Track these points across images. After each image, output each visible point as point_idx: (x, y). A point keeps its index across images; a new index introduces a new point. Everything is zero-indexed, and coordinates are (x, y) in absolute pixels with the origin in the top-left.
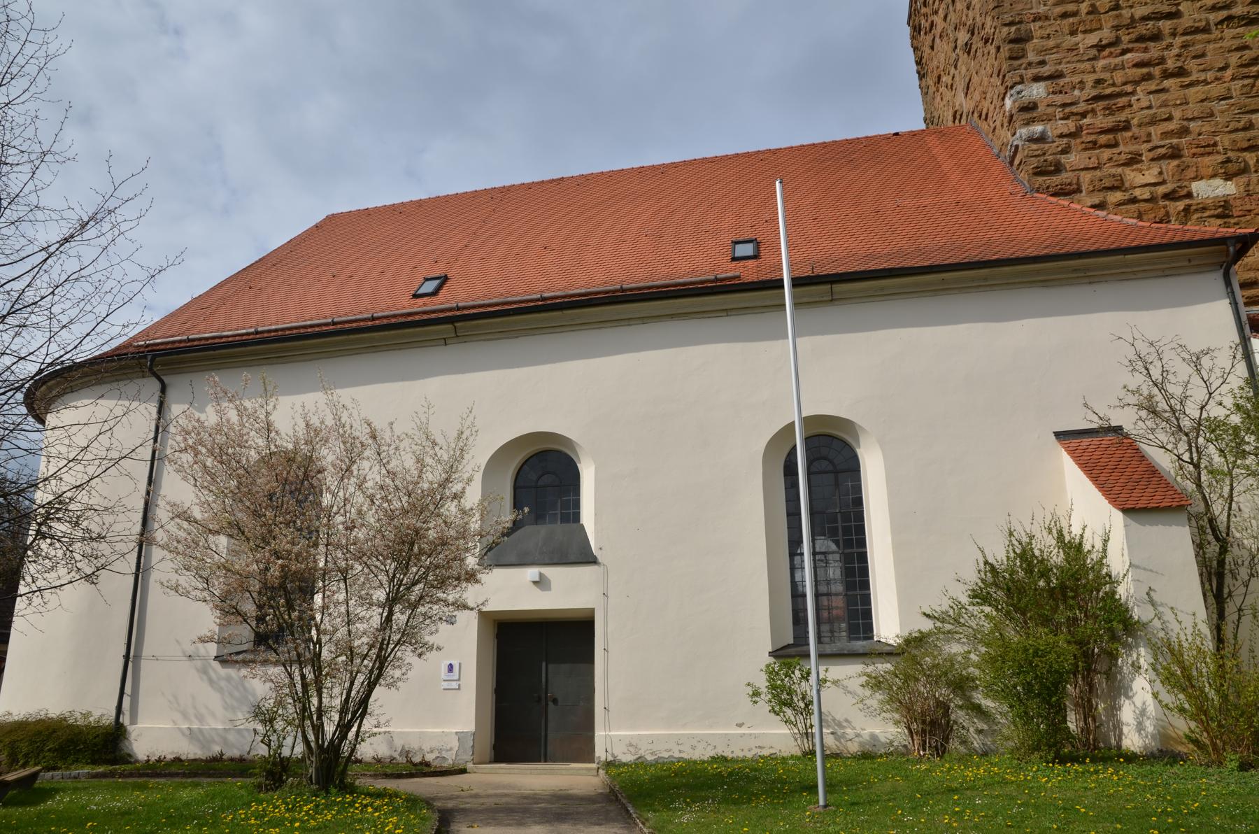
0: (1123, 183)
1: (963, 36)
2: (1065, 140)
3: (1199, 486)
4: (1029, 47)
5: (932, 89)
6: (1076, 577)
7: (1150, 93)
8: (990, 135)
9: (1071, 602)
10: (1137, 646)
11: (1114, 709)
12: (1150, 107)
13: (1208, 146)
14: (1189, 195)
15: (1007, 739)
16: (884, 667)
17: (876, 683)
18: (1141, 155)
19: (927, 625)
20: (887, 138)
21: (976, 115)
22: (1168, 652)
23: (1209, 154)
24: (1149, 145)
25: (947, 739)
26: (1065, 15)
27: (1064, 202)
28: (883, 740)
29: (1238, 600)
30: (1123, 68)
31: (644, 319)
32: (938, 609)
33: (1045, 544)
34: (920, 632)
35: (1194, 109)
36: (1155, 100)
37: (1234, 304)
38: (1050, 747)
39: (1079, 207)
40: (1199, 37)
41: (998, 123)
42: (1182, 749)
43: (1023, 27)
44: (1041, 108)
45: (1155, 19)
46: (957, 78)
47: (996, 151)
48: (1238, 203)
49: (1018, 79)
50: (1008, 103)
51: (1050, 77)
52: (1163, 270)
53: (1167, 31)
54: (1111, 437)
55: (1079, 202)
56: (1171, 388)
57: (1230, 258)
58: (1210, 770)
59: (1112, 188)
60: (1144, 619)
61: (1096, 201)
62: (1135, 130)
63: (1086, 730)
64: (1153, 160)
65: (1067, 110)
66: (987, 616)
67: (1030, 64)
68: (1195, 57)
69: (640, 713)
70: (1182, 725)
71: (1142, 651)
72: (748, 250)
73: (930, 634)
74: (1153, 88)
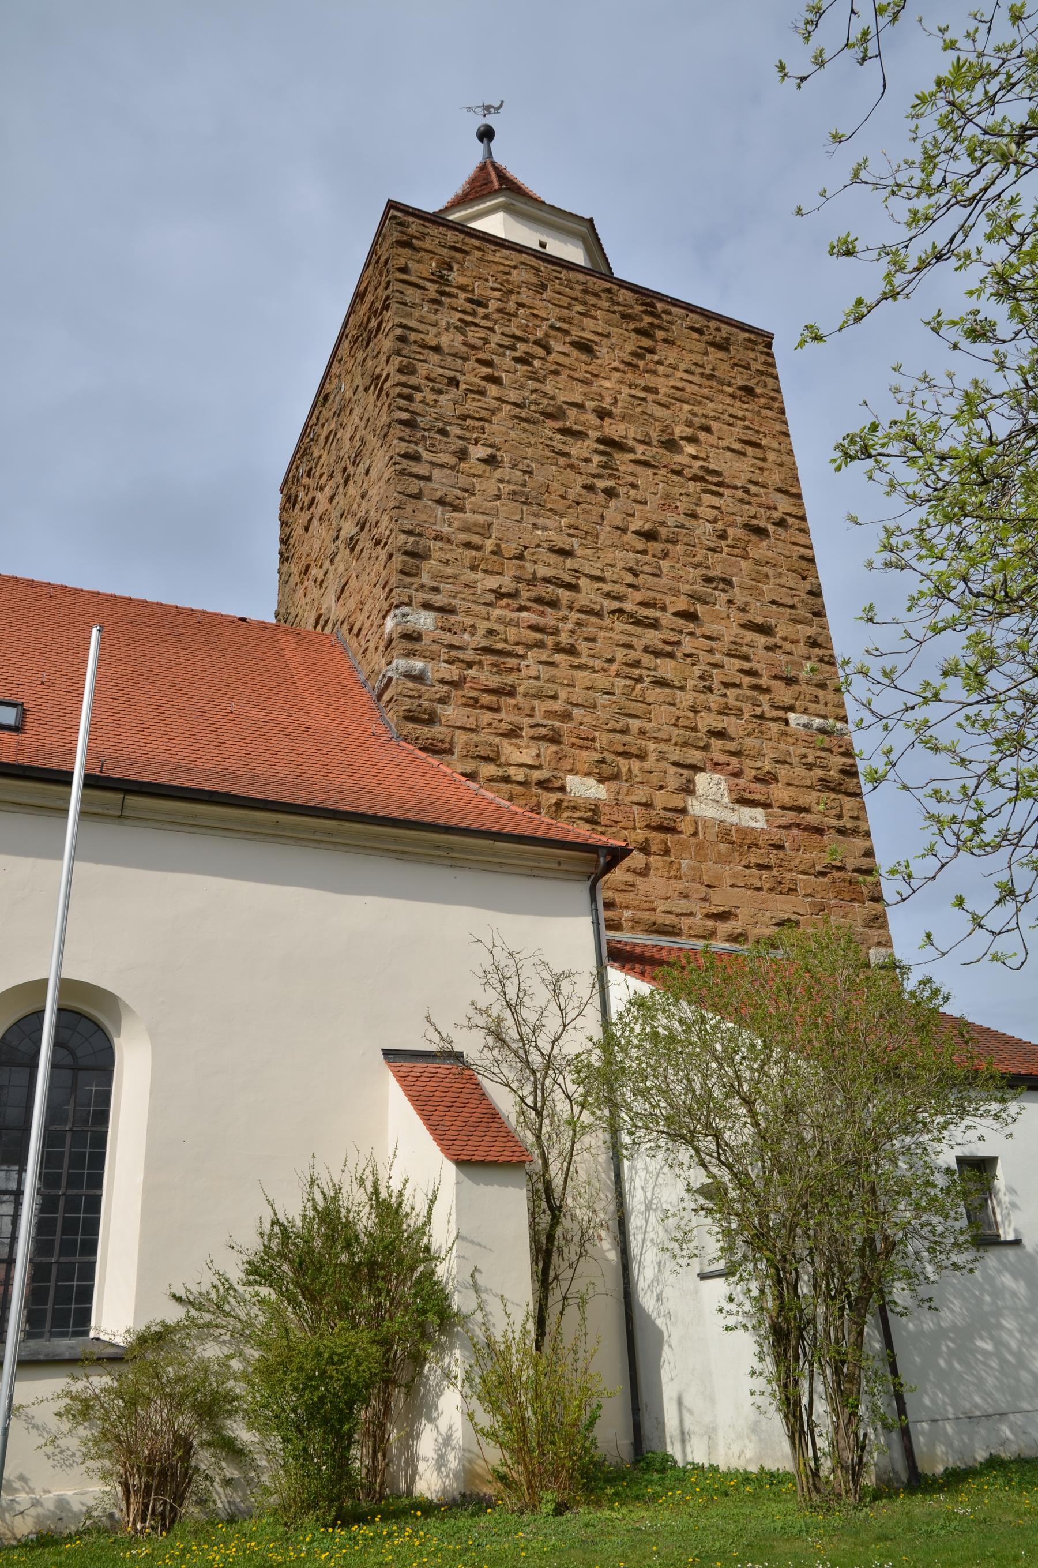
0: (498, 756)
1: (349, 528)
2: (446, 688)
3: (538, 1138)
4: (425, 566)
5: (295, 579)
6: (390, 1249)
7: (540, 662)
8: (359, 657)
9: (380, 1284)
10: (452, 1348)
11: (411, 1436)
12: (537, 678)
13: (587, 739)
14: (562, 789)
15: (266, 1491)
16: (100, 1381)
17: (82, 1409)
18: (521, 729)
19: (175, 1314)
20: (230, 621)
21: (345, 626)
22: (487, 1351)
23: (587, 748)
24: (531, 721)
25: (179, 1498)
26: (468, 545)
27: (433, 760)
28: (76, 1507)
29: (564, 1285)
30: (518, 626)
32: (195, 1289)
33: (356, 1203)
34: (164, 1324)
35: (579, 695)
36: (545, 672)
37: (596, 923)
38: (331, 1500)
39: (449, 771)
40: (593, 619)
41: (372, 645)
42: (488, 1490)
43: (422, 541)
44: (426, 642)
45: (555, 584)
46: (330, 575)
47: (362, 677)
48: (607, 810)
50: (389, 623)
51: (440, 609)
52: (532, 868)
53: (564, 602)
54: (447, 1066)
55: (449, 765)
56: (525, 1013)
57: (599, 871)
58: (525, 1518)
60: (465, 1310)
62: (519, 698)
63: (373, 1471)
64: (532, 738)
65: (454, 653)
67: (422, 586)
68: (586, 639)
70: (494, 1455)
71: (457, 1353)
73: (178, 1327)
74: (544, 658)
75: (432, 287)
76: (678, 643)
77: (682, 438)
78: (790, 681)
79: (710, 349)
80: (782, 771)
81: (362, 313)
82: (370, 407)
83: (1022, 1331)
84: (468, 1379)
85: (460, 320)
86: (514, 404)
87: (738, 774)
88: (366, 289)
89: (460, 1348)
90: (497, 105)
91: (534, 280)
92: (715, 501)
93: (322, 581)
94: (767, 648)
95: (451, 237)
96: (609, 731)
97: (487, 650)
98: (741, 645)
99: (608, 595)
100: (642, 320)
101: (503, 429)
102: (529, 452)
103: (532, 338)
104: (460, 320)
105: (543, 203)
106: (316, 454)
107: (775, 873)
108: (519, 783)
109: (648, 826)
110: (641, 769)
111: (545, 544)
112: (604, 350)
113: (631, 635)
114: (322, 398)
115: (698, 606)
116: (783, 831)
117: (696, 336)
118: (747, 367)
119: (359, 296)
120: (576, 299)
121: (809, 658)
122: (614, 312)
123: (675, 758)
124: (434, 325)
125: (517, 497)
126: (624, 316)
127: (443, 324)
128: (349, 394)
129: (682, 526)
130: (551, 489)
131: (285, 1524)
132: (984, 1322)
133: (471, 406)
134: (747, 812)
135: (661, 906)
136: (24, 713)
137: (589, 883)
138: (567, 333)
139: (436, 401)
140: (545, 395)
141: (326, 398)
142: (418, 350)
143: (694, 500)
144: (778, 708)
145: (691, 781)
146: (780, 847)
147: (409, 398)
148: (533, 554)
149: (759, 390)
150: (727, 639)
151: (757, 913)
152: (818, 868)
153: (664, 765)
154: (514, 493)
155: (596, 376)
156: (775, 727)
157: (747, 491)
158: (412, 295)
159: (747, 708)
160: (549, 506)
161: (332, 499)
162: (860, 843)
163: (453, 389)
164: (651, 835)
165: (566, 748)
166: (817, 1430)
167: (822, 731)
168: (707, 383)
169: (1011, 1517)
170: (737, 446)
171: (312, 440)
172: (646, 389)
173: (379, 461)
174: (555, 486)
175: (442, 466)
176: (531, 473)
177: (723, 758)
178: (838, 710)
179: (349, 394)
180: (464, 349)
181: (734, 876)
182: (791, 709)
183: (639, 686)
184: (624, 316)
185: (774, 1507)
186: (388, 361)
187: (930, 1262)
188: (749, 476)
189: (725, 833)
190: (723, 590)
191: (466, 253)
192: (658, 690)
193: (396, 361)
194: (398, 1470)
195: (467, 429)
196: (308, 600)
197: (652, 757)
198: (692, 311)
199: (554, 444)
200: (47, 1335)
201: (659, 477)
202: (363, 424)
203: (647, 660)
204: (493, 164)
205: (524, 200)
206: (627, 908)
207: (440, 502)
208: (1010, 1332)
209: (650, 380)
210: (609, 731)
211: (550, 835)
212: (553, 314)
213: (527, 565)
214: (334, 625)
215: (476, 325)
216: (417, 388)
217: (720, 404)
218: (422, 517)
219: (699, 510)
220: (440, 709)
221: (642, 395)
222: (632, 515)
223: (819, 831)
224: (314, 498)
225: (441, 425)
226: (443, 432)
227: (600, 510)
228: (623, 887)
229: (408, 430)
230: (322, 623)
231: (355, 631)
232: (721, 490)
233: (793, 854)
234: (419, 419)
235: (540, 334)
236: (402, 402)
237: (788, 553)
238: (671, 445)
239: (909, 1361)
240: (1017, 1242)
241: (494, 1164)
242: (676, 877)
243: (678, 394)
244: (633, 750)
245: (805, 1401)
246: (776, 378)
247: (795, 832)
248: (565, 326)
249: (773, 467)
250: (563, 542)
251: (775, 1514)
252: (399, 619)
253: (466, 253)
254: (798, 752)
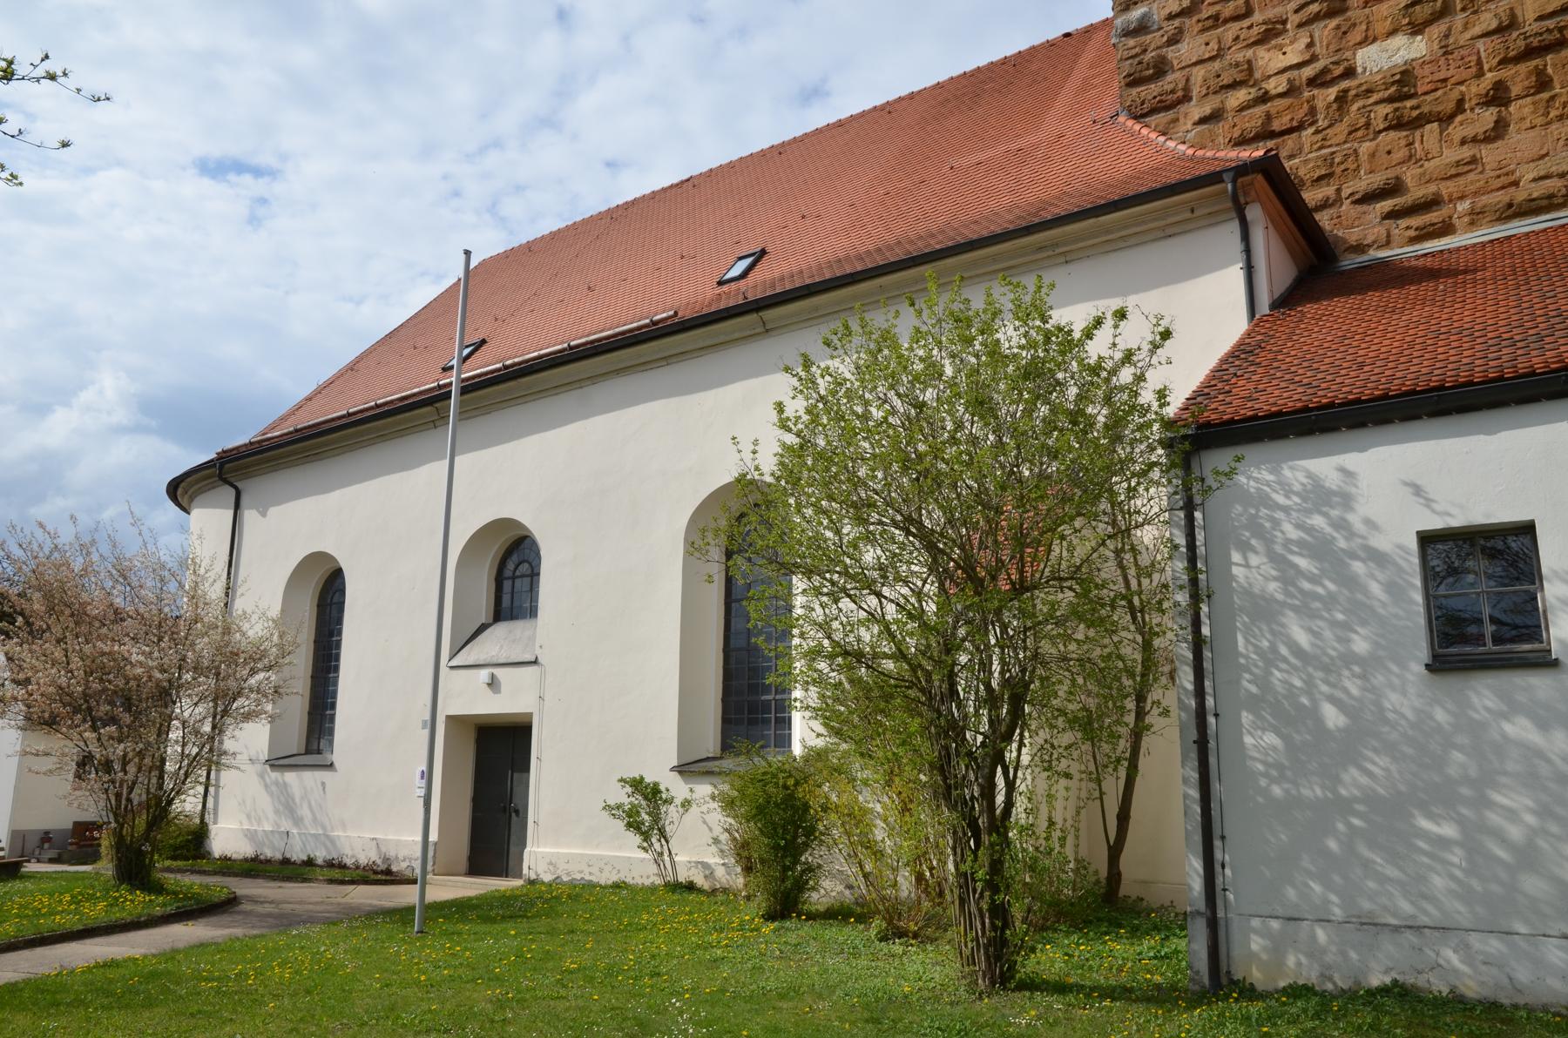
2: (1177, 23)
14: (1350, 73)
18: (1284, 22)
31: (594, 379)
52: (1163, 228)
59: (1234, 85)
61: (1207, 110)
64: (1300, 25)
69: (569, 835)
108: (1281, 95)
135: (1528, 173)
206: (1462, 198)
208: (1512, 815)
220: (1170, 53)
228: (1453, 171)
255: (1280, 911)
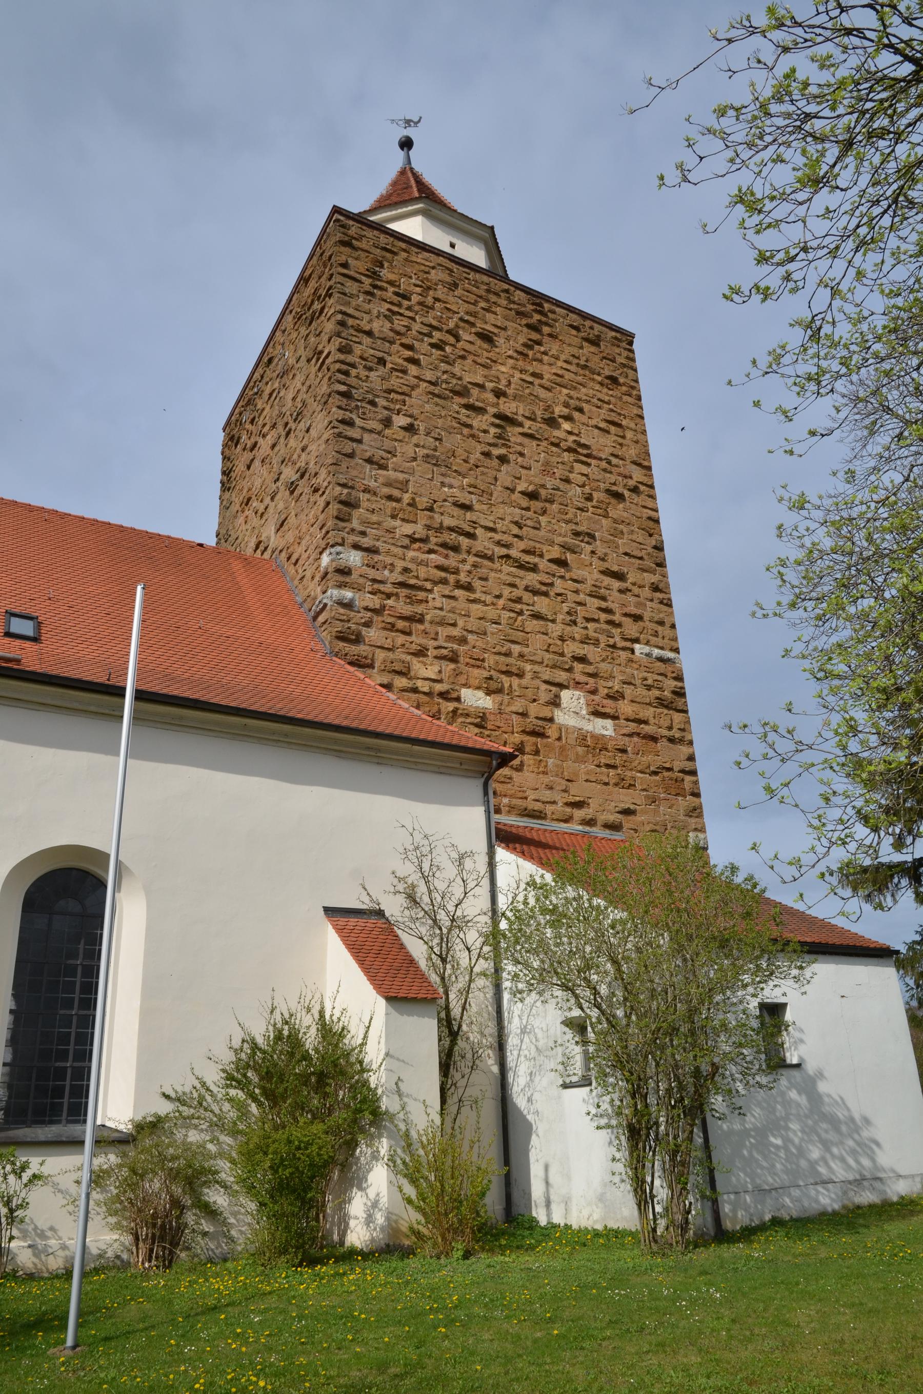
0: (409, 671)
2: (369, 614)
4: (356, 513)
5: (235, 507)
7: (444, 596)
8: (296, 582)
10: (380, 1136)
12: (441, 609)
13: (478, 660)
14: (458, 699)
19: (164, 1108)
23: (478, 667)
24: (436, 644)
26: (390, 498)
29: (461, 1091)
30: (427, 566)
32: (180, 1089)
35: (473, 624)
37: (488, 812)
38: (297, 1248)
40: (486, 562)
41: (308, 574)
43: (354, 493)
44: (354, 576)
46: (271, 510)
47: (299, 599)
49: (340, 541)
50: (325, 560)
51: (366, 550)
52: (439, 767)
53: (464, 547)
62: (427, 625)
64: (436, 657)
65: (376, 586)
66: (231, 1100)
67: (353, 530)
68: (480, 579)
70: (412, 1217)
72: (24, 627)
74: (447, 593)
75: (367, 281)
76: (551, 585)
77: (560, 417)
78: (637, 618)
79: (585, 344)
80: (628, 691)
81: (306, 294)
82: (312, 376)
83: (803, 1131)
84: (392, 1159)
85: (389, 310)
86: (430, 382)
87: (594, 692)
88: (310, 275)
89: (388, 1137)
90: (416, 120)
91: (448, 279)
92: (585, 469)
93: (262, 514)
94: (621, 591)
95: (383, 239)
96: (496, 653)
97: (403, 585)
98: (600, 587)
99: (499, 543)
100: (532, 317)
101: (420, 402)
102: (440, 422)
103: (445, 327)
104: (389, 310)
105: (455, 211)
106: (259, 406)
107: (619, 771)
108: (425, 693)
109: (524, 732)
110: (519, 686)
111: (450, 499)
112: (502, 341)
113: (515, 576)
114: (265, 360)
115: (568, 555)
116: (627, 739)
117: (574, 332)
118: (613, 361)
119: (303, 280)
120: (481, 297)
121: (652, 600)
122: (510, 309)
123: (546, 678)
124: (368, 312)
125: (429, 460)
126: (518, 313)
127: (375, 312)
128: (292, 361)
129: (558, 489)
130: (457, 454)
131: (263, 1265)
132: (776, 1125)
133: (395, 382)
134: (600, 722)
135: (532, 796)
136: (39, 625)
137: (483, 780)
138: (473, 325)
139: (367, 377)
140: (454, 376)
141: (270, 361)
142: (355, 333)
143: (568, 468)
144: (626, 640)
145: (557, 696)
146: (624, 751)
147: (346, 373)
148: (441, 507)
149: (621, 380)
150: (590, 582)
151: (605, 803)
152: (652, 768)
153: (537, 682)
154: (428, 456)
155: (495, 362)
156: (624, 655)
157: (609, 463)
158: (351, 287)
159: (603, 639)
160: (454, 468)
161: (273, 446)
162: (685, 750)
163: (381, 367)
164: (526, 738)
165: (462, 666)
166: (655, 1200)
167: (660, 659)
168: (582, 372)
169: (790, 1258)
170: (603, 425)
171: (256, 394)
172: (534, 375)
173: (320, 423)
174: (459, 451)
175: (371, 431)
176: (441, 440)
177: (583, 679)
178: (673, 643)
179: (292, 361)
180: (391, 334)
181: (588, 773)
182: (637, 641)
183: (520, 618)
184: (518, 313)
185: (625, 1254)
186: (329, 341)
187: (741, 1081)
188: (611, 450)
189: (582, 738)
190: (588, 543)
191: (395, 253)
192: (535, 622)
193: (337, 342)
194: (331, 1227)
195: (392, 401)
196: (248, 527)
197: (528, 676)
198: (572, 312)
199: (460, 416)
200: (64, 1122)
201: (541, 448)
202: (305, 389)
203: (527, 597)
204: (412, 169)
205: (439, 207)
207: (369, 461)
208: (795, 1132)
209: (535, 367)
210: (496, 653)
211: (455, 742)
212: (463, 309)
213: (436, 516)
214: (273, 552)
215: (401, 315)
216: (353, 366)
217: (591, 390)
218: (354, 473)
219: (572, 476)
220: (364, 631)
221: (530, 379)
222: (519, 478)
223: (654, 739)
224: (256, 443)
225: (370, 397)
226: (373, 403)
227: (494, 473)
229: (345, 400)
230: (261, 548)
231: (293, 559)
232: (589, 460)
233: (634, 756)
234: (354, 391)
235: (451, 325)
236: (341, 377)
237: (638, 514)
238: (552, 422)
239: (721, 1153)
240: (798, 1066)
241: (414, 1000)
242: (543, 773)
243: (559, 380)
244: (514, 670)
245: (649, 1179)
246: (636, 370)
247: (636, 739)
248: (472, 319)
249: (631, 443)
250: (464, 498)
251: (628, 1258)
252: (334, 556)
253: (395, 253)
254: (641, 676)
255: (731, 1190)
